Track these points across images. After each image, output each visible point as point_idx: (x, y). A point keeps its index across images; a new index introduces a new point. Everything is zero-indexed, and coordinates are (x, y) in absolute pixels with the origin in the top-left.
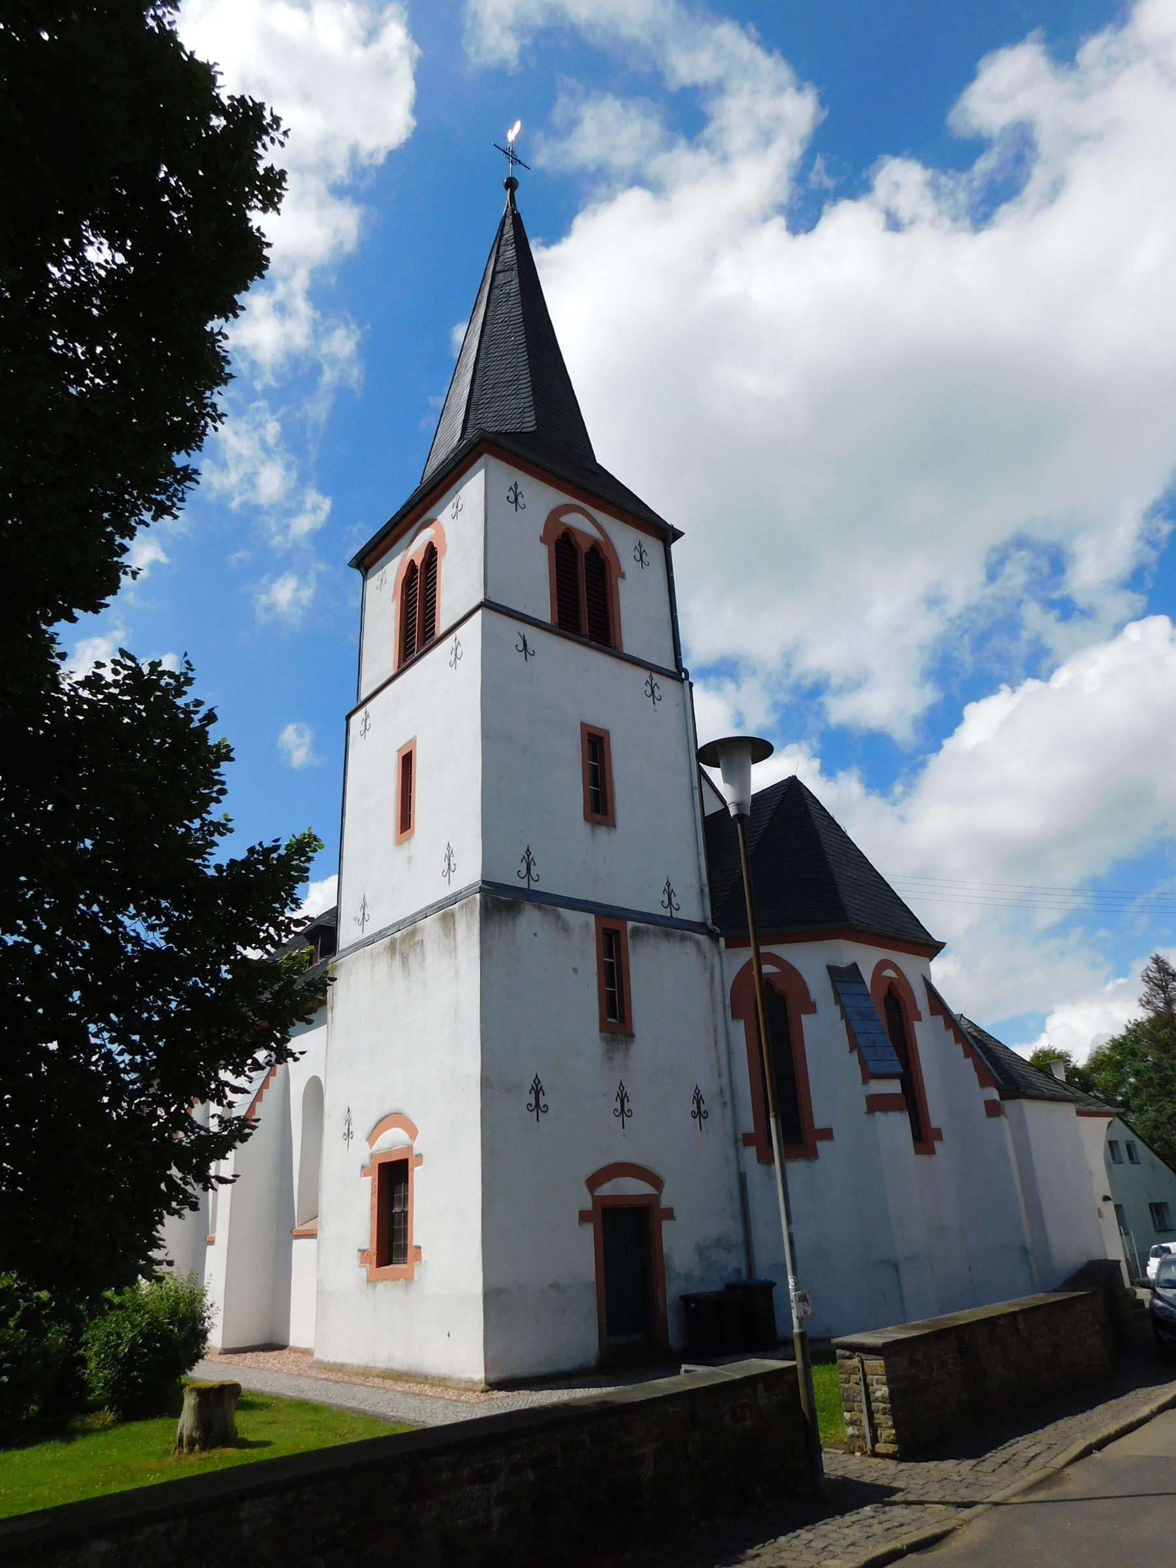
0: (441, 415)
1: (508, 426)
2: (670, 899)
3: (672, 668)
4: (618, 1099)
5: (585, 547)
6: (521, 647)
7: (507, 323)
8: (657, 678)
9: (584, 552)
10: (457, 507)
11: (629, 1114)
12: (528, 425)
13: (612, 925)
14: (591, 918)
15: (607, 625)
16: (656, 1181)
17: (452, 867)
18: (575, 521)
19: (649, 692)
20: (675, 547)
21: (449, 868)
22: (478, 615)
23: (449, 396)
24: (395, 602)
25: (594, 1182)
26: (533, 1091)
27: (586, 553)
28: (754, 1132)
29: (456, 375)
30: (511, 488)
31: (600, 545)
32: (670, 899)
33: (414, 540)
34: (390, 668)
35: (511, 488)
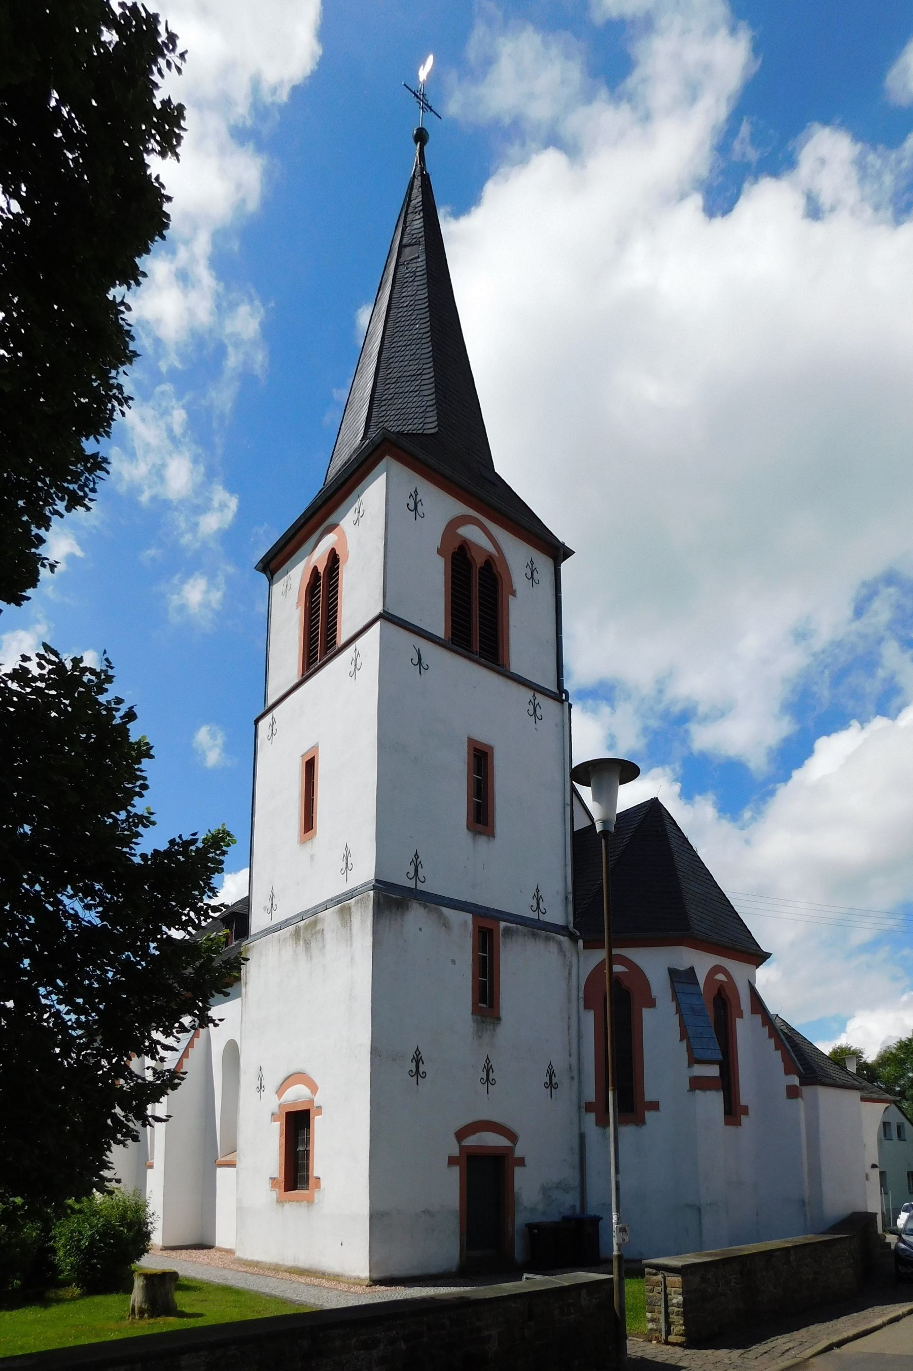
3: (554, 689)
5: (479, 561)
6: (416, 661)
8: (540, 698)
11: (493, 1082)
12: (430, 426)
13: (487, 924)
14: (469, 917)
16: (512, 1136)
18: (471, 533)
19: (532, 712)
20: (565, 566)
21: (347, 867)
24: (299, 608)
25: (461, 1134)
26: (414, 1061)
30: (411, 495)
32: (538, 904)
35: (411, 495)
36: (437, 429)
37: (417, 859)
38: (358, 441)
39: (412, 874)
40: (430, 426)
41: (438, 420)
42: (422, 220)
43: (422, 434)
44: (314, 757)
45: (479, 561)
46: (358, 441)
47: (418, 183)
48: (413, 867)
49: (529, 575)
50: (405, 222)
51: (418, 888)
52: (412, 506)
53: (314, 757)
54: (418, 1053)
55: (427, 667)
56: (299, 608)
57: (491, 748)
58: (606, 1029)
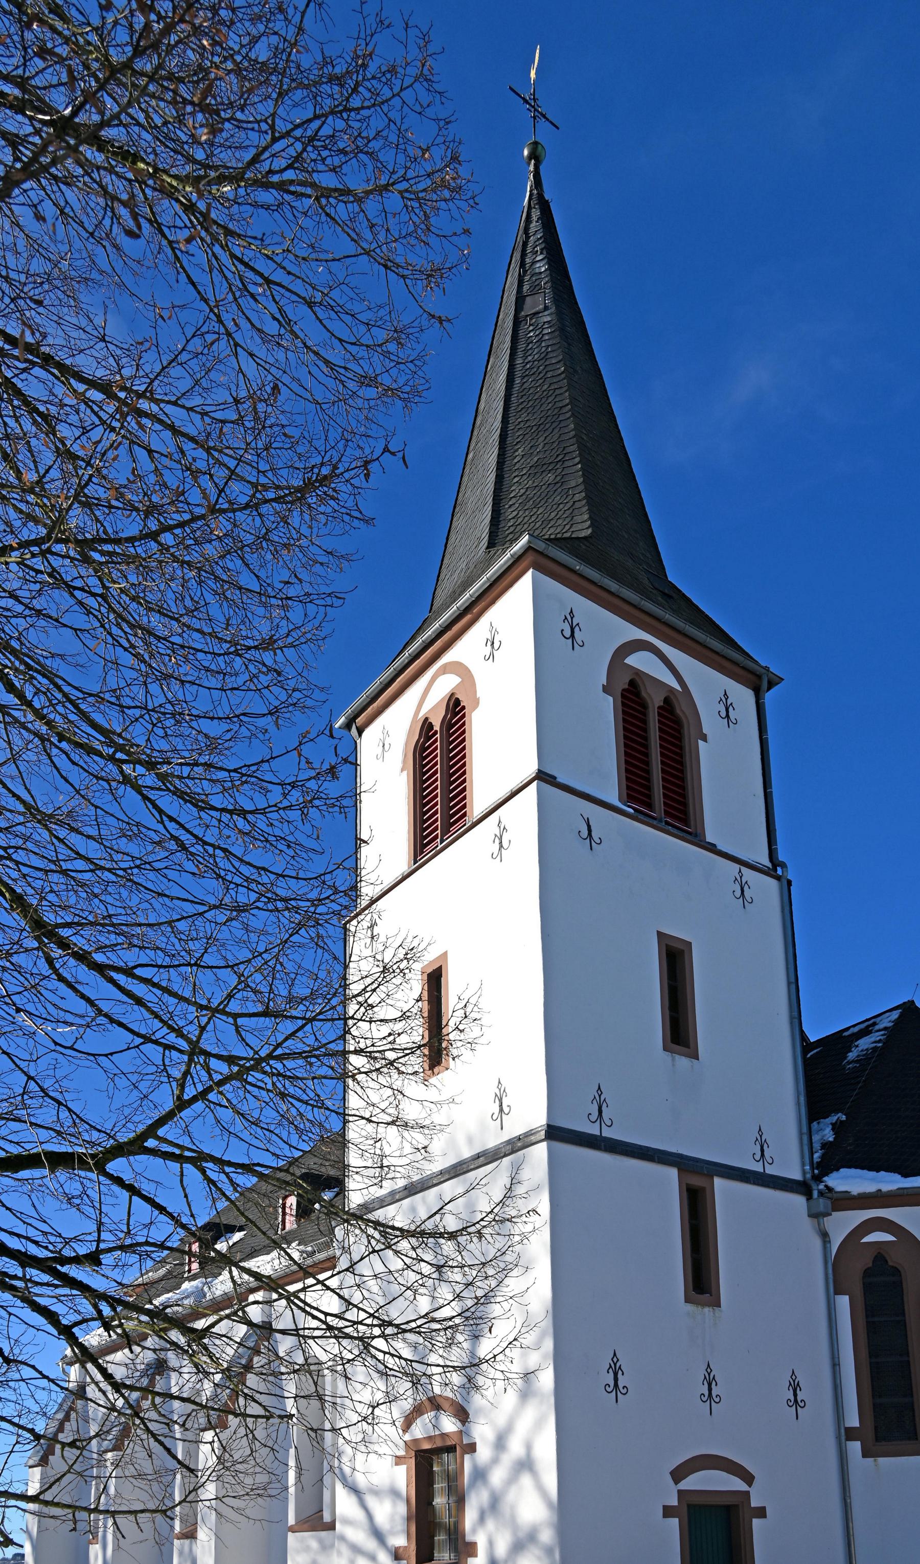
0: (453, 515)
1: (552, 530)
2: (762, 1151)
3: (766, 862)
4: (705, 1382)
5: (656, 700)
6: (585, 833)
7: (542, 375)
8: (748, 873)
9: (657, 706)
10: (493, 643)
11: (717, 1400)
12: (580, 527)
13: (696, 1181)
14: (673, 1172)
15: (685, 805)
16: (748, 1478)
17: (506, 1110)
18: (638, 661)
19: (738, 893)
20: (769, 697)
21: (501, 1110)
22: (534, 785)
23: (463, 488)
24: (405, 773)
25: (678, 1475)
26: (611, 1370)
27: (659, 708)
28: (754, 1520)
29: (470, 456)
30: (566, 618)
31: (675, 696)
32: (762, 1151)
33: (732, 640)
34: (403, 866)
35: (566, 618)
36: (590, 531)
37: (600, 1096)
38: (481, 552)
39: (594, 1116)
40: (580, 527)
41: (590, 518)
42: (546, 261)
43: (570, 538)
44: (441, 967)
45: (656, 700)
46: (481, 552)
47: (536, 214)
48: (595, 1107)
49: (724, 714)
50: (522, 264)
51: (603, 1135)
52: (568, 633)
53: (441, 967)
54: (615, 1360)
55: (599, 841)
56: (405, 773)
57: (689, 944)
58: (835, 1365)
